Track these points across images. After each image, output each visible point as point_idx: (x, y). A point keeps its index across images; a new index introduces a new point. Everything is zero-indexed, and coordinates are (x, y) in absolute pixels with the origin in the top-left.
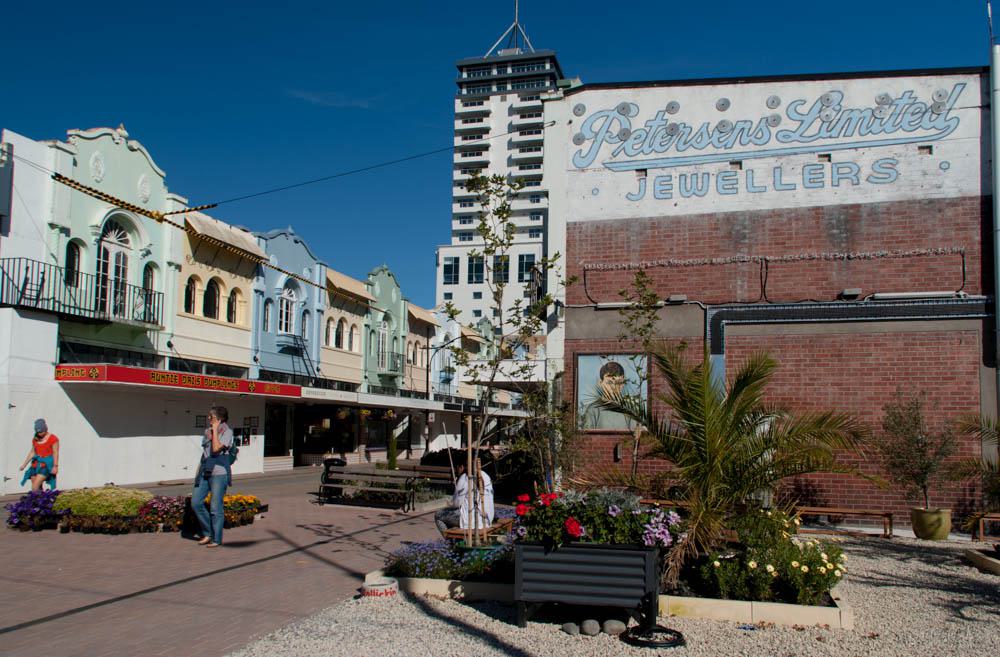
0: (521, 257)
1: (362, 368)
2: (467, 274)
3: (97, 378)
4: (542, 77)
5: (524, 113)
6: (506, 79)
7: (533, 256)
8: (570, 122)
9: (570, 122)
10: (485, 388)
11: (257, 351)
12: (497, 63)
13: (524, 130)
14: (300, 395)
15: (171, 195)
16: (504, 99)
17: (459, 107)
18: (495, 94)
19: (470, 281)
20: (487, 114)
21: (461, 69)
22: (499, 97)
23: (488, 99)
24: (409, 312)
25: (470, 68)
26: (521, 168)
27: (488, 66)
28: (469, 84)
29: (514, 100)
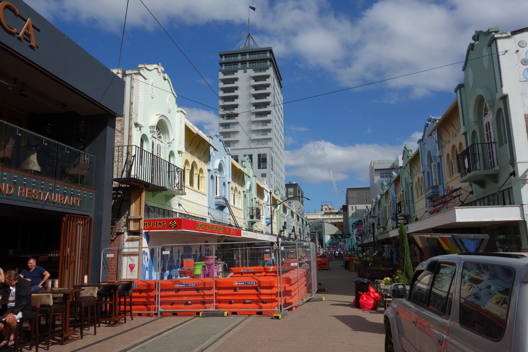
0: (259, 155)
1: (243, 218)
2: (257, 164)
3: (176, 227)
4: (236, 63)
5: (256, 79)
6: (246, 61)
7: (266, 154)
8: (517, 51)
9: (517, 51)
10: (486, 236)
11: (209, 208)
12: (241, 53)
13: (256, 96)
14: (240, 235)
15: (180, 109)
16: (245, 72)
17: (221, 76)
18: (240, 69)
19: (259, 167)
20: (236, 79)
21: (221, 56)
22: (243, 71)
23: (237, 71)
24: (257, 184)
25: (226, 55)
26: (255, 81)
27: (236, 54)
28: (226, 64)
29: (251, 72)
